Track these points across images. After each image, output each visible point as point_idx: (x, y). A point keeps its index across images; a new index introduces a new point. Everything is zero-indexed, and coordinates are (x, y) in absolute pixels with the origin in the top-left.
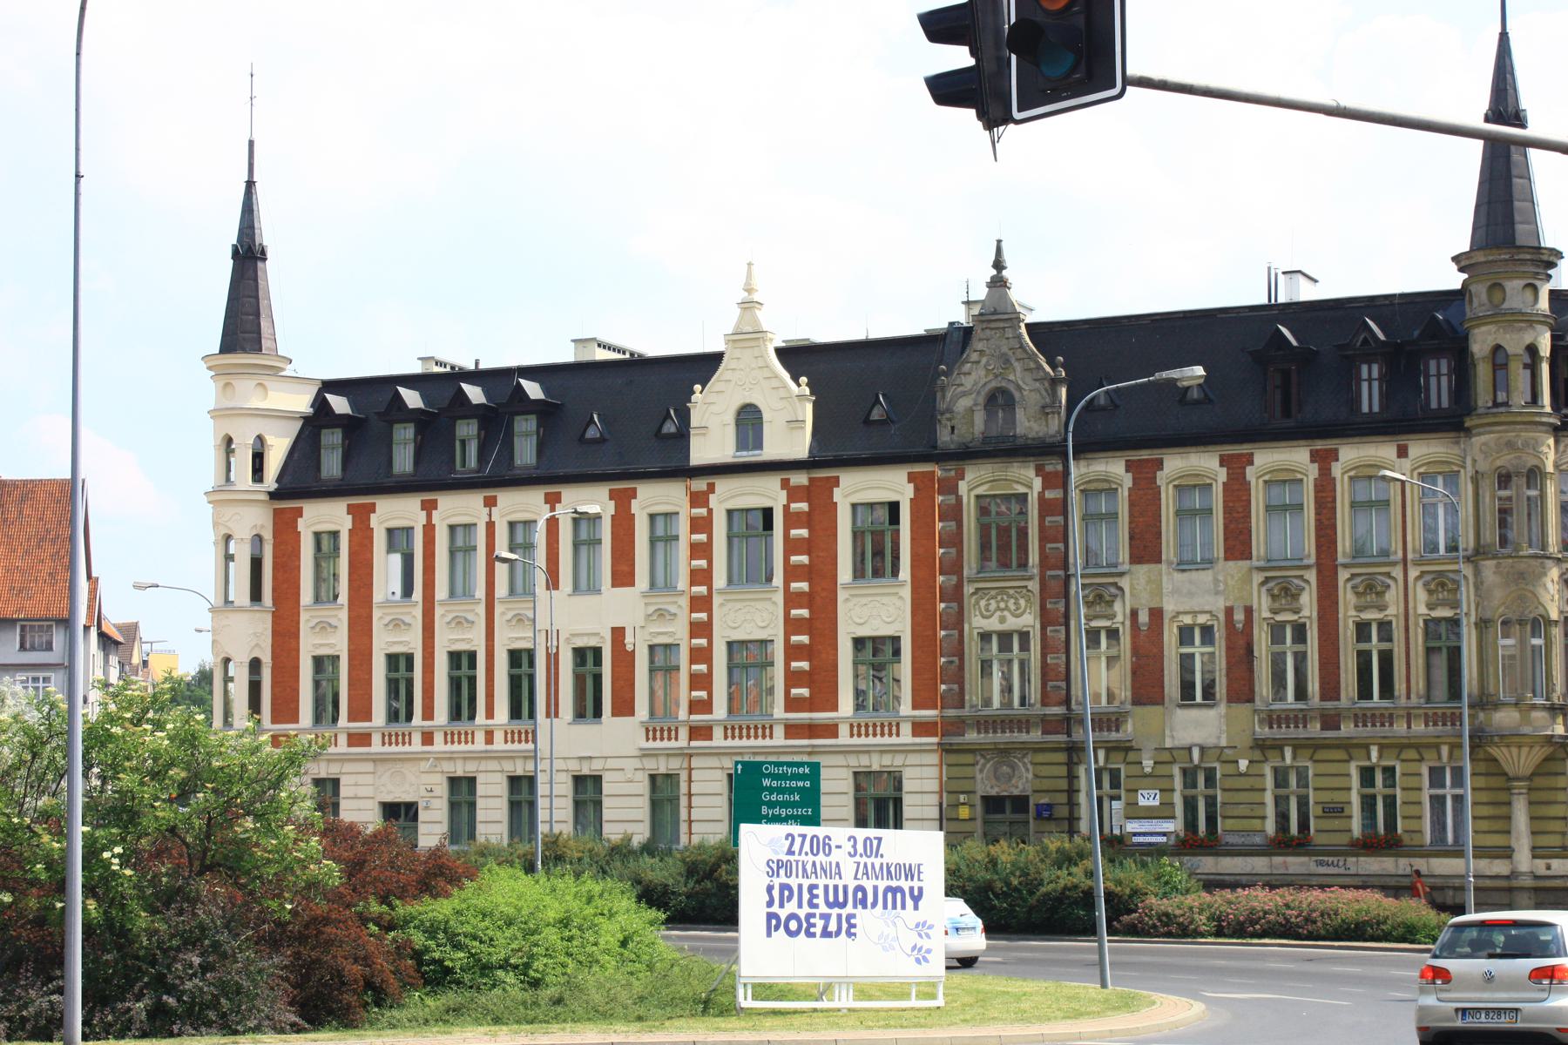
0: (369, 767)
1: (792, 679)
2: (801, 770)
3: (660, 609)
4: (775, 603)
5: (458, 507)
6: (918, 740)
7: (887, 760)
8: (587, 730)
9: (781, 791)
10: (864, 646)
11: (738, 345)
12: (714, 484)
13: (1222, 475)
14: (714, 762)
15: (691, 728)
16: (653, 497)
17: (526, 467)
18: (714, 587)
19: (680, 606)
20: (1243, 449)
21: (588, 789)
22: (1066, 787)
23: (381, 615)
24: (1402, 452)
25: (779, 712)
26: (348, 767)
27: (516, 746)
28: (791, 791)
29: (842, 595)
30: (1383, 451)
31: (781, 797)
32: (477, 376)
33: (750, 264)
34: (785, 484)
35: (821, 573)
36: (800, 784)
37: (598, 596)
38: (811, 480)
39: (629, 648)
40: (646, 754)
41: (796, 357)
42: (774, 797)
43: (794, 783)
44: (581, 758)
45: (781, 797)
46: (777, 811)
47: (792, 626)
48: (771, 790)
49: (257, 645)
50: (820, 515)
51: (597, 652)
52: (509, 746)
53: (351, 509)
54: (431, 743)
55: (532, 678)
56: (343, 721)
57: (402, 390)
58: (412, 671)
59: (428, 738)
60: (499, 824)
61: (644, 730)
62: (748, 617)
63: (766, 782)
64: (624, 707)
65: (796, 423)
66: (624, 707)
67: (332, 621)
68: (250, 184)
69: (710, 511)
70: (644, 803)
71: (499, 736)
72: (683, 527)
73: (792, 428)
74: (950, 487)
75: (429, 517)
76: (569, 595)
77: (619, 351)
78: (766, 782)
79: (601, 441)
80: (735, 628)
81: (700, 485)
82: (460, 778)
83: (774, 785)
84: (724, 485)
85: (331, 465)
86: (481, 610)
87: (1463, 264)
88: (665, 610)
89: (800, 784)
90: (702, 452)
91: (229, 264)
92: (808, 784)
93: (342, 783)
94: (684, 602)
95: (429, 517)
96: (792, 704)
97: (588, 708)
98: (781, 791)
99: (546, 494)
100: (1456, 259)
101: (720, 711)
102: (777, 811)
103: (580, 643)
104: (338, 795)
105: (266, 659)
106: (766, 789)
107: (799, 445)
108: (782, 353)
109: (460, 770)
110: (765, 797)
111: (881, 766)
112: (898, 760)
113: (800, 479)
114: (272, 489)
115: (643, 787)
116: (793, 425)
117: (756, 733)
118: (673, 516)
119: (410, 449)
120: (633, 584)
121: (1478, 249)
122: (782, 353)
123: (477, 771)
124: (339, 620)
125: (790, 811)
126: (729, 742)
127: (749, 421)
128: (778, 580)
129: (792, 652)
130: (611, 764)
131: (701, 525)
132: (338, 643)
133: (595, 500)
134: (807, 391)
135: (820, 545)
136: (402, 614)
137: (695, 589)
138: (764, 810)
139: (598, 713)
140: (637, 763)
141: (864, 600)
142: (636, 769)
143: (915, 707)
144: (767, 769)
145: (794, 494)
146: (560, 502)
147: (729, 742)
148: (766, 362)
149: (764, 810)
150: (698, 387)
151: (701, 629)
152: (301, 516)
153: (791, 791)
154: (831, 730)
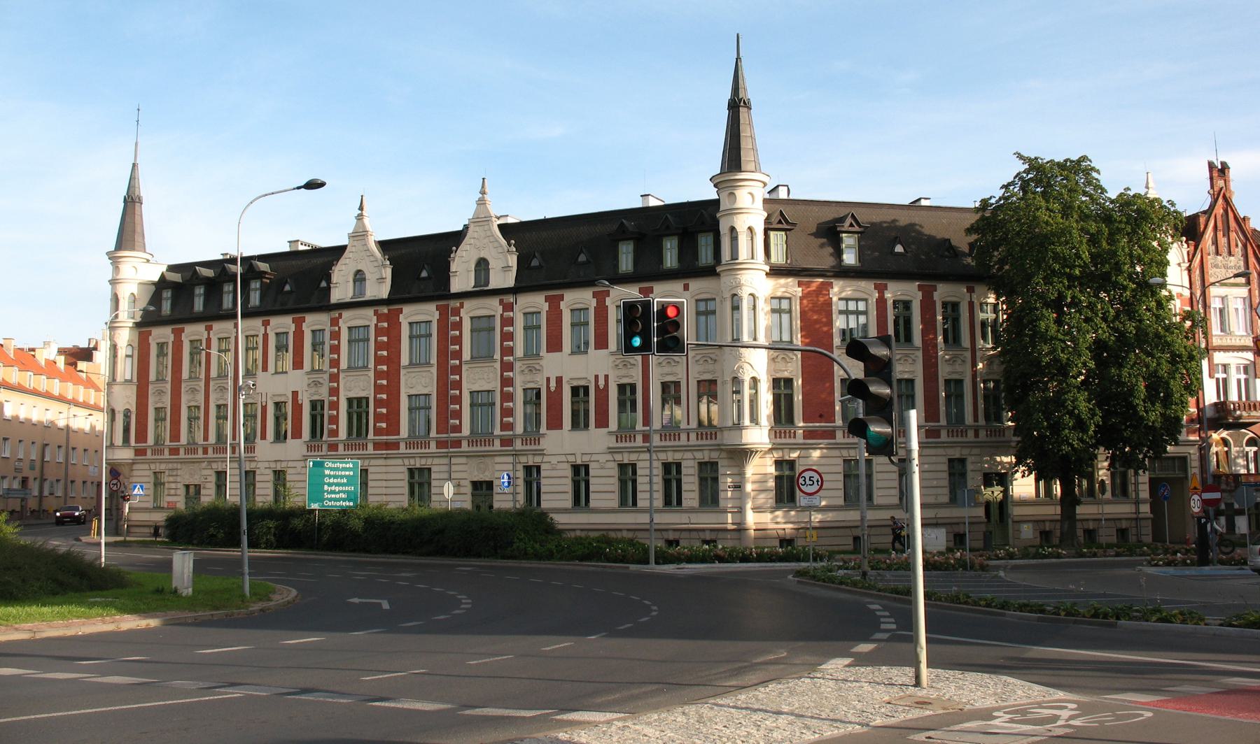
0: (463, 460)
1: (378, 418)
2: (348, 466)
3: (529, 367)
4: (431, 373)
5: (194, 331)
6: (439, 451)
7: (423, 461)
8: (580, 435)
9: (335, 477)
10: (247, 406)
11: (355, 239)
12: (463, 303)
13: (546, 306)
14: (399, 462)
15: (329, 445)
16: (314, 321)
17: (227, 310)
18: (463, 360)
19: (324, 380)
20: (180, 326)
21: (580, 473)
22: (648, 474)
23: (694, 355)
24: (686, 288)
25: (497, 432)
26: (373, 462)
27: (704, 442)
28: (342, 477)
29: (403, 372)
30: (677, 286)
31: (335, 481)
32: (263, 258)
33: (362, 196)
34: (376, 313)
35: (393, 360)
36: (347, 473)
37: (585, 356)
38: (389, 310)
39: (300, 402)
40: (612, 451)
41: (507, 230)
42: (332, 480)
43: (343, 473)
44: (276, 461)
45: (335, 481)
46: (333, 488)
47: (378, 389)
48: (330, 476)
49: (128, 402)
50: (393, 331)
51: (586, 389)
52: (700, 442)
53: (173, 331)
54: (207, 454)
55: (367, 413)
56: (371, 436)
57: (197, 268)
58: (540, 398)
59: (205, 451)
60: (693, 492)
61: (306, 446)
62: (357, 384)
63: (327, 472)
64: (602, 422)
65: (381, 280)
66: (297, 434)
67: (537, 367)
68: (738, 59)
69: (461, 318)
70: (405, 484)
71: (210, 450)
72: (327, 335)
73: (505, 271)
74: (456, 312)
75: (209, 334)
76: (569, 355)
77: (305, 245)
78: (327, 472)
79: (540, 267)
80: (426, 387)
81: (335, 314)
82: (626, 465)
83: (332, 473)
84: (346, 314)
85: (166, 307)
86: (202, 384)
87: (111, 256)
88: (318, 381)
89: (347, 473)
90: (336, 296)
91: (122, 205)
92: (351, 473)
93: (542, 468)
94: (326, 376)
95: (209, 334)
96: (378, 432)
97: (579, 422)
98: (335, 477)
99: (594, 293)
100: (108, 253)
101: (343, 434)
102: (333, 488)
103: (575, 383)
104: (681, 474)
105: (133, 409)
106: (327, 476)
107: (384, 291)
108: (502, 227)
109: (419, 463)
110: (327, 480)
111: (582, 462)
112: (429, 461)
113: (384, 310)
114: (138, 321)
115: (615, 472)
116: (380, 281)
117: (780, 435)
118: (491, 318)
119: (169, 302)
120: (302, 368)
121: (145, 249)
122: (502, 227)
123: (682, 459)
124: (167, 389)
125: (341, 488)
126: (408, 451)
127: (482, 266)
128: (497, 356)
129: (379, 403)
130: (290, 464)
131: (336, 335)
132: (167, 401)
133: (284, 323)
134: (514, 249)
135: (393, 345)
136: (711, 353)
137: (332, 370)
138: (326, 487)
139: (587, 426)
140: (609, 457)
141: (413, 375)
142: (266, 468)
143: (170, 442)
144: (327, 465)
145: (380, 317)
146: (609, 296)
147: (408, 451)
148: (492, 233)
149: (326, 487)
150: (454, 248)
151: (334, 392)
152: (563, 300)
153: (342, 477)
154: (396, 445)
